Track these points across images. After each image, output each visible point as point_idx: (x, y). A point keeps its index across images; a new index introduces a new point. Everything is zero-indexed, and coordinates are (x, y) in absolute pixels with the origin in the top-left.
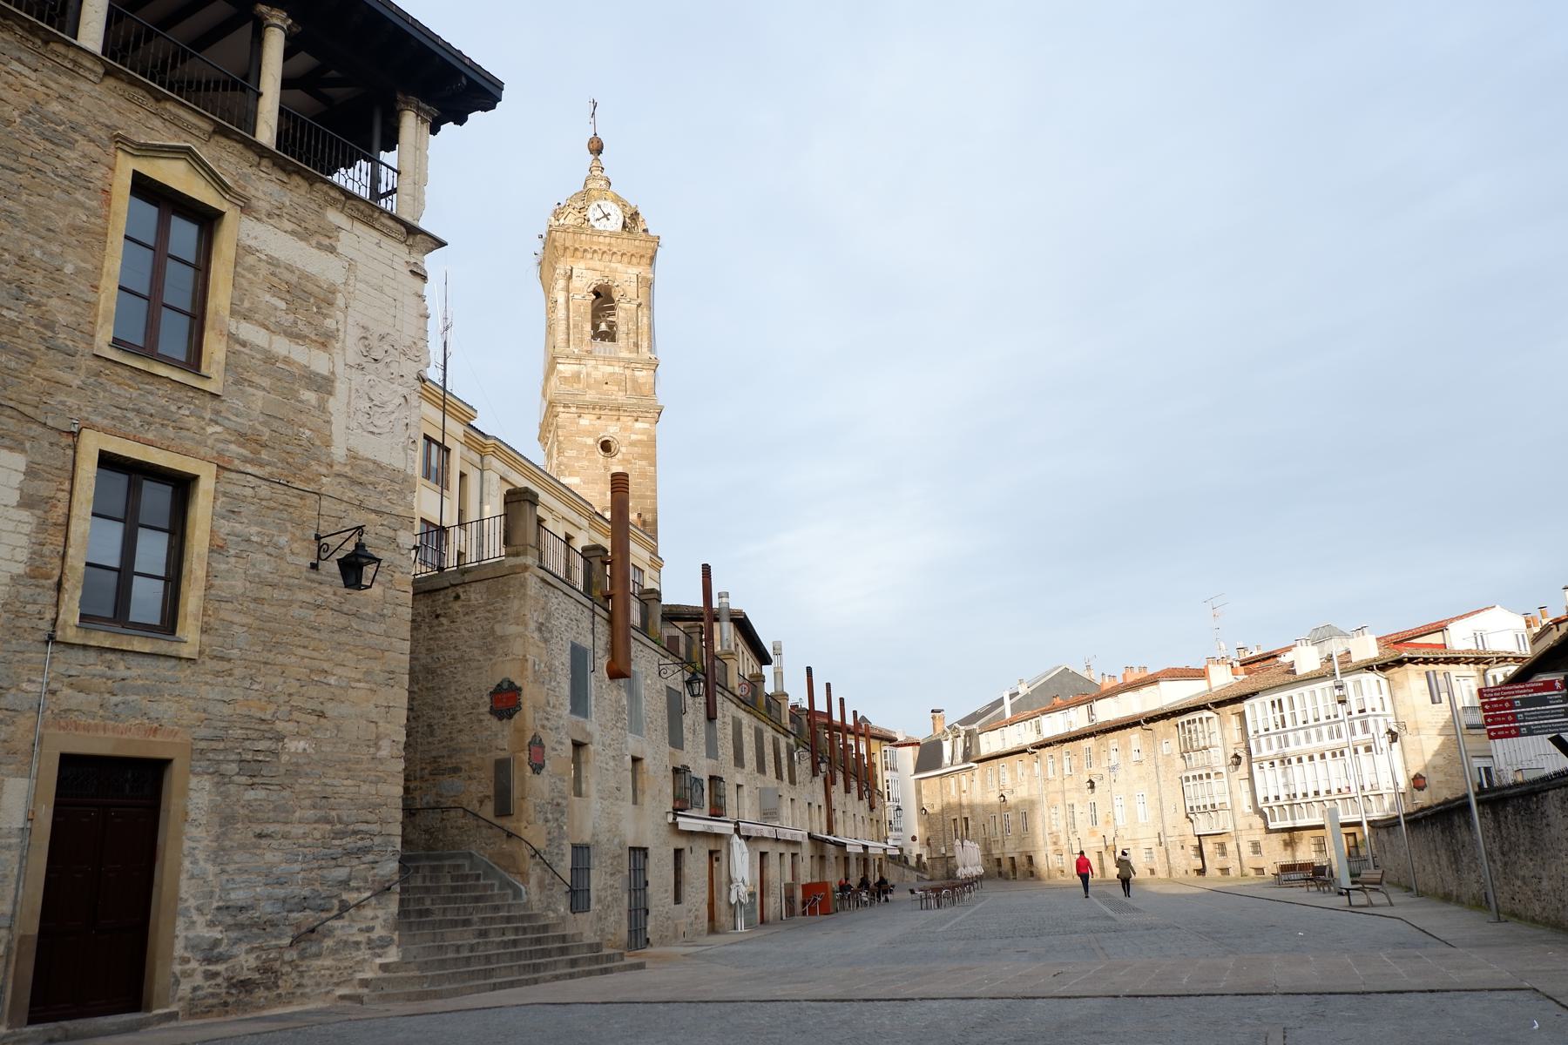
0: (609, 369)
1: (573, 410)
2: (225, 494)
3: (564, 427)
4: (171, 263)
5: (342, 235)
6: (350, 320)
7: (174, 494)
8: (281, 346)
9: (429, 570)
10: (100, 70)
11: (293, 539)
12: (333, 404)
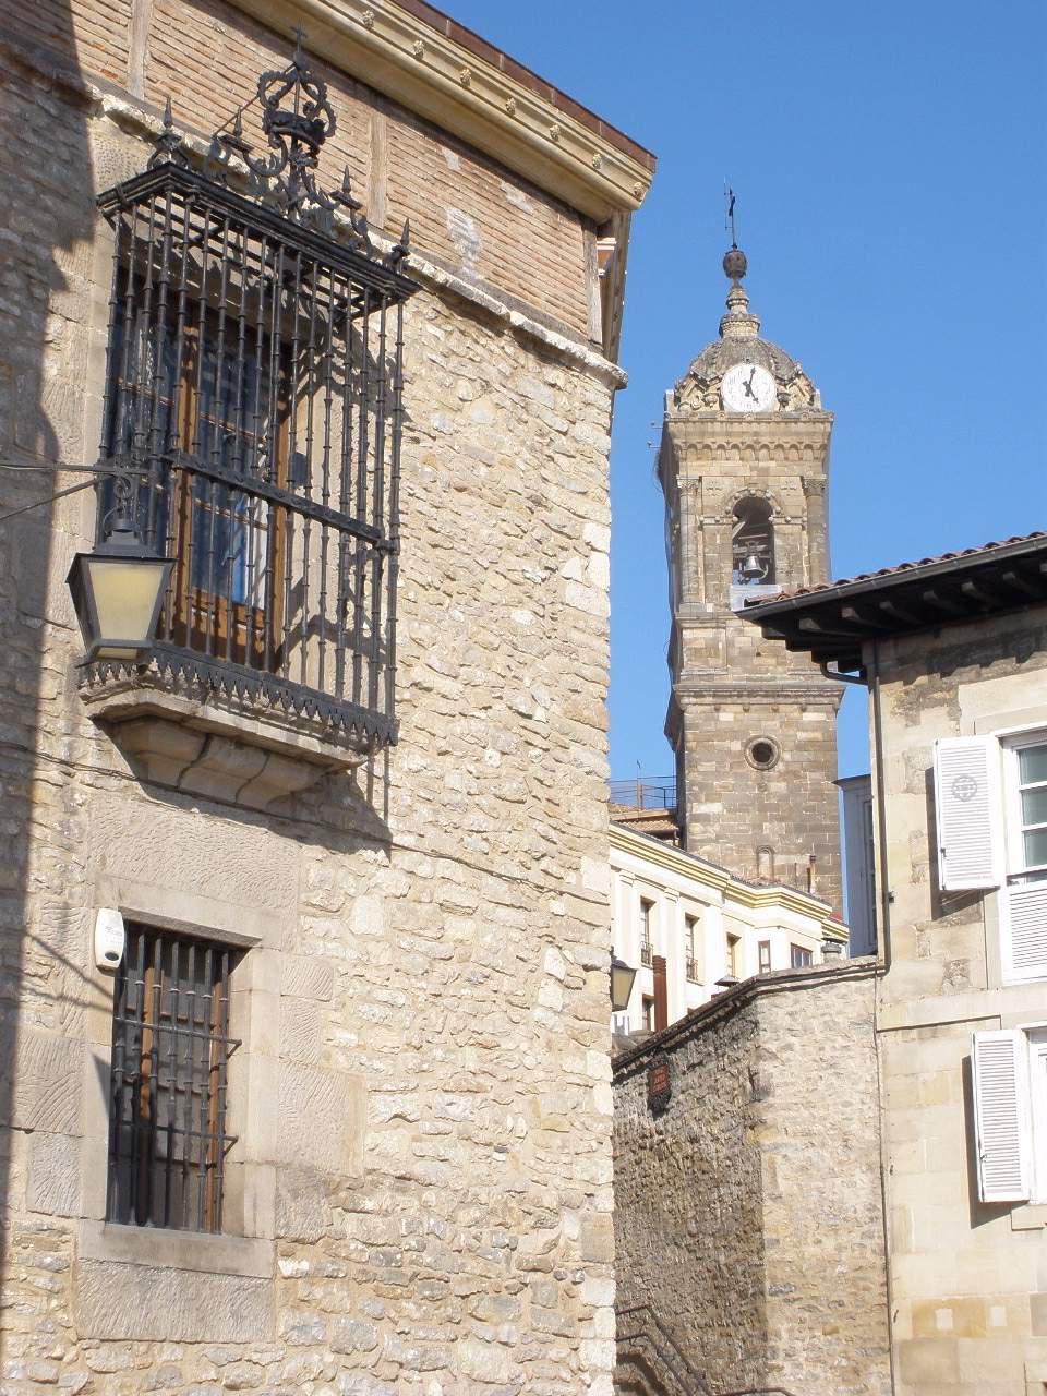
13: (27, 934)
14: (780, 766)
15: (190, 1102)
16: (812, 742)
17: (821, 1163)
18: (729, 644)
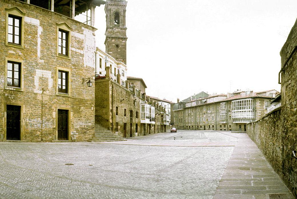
0: (118, 30)
1: (111, 39)
2: (72, 74)
3: (109, 42)
4: (63, 40)
5: (84, 31)
6: (86, 45)
7: (66, 74)
8: (77, 51)
9: (49, 42)
10: (54, 14)
11: (80, 79)
12: (84, 58)
13: (19, 27)
14: (120, 48)
15: (198, 115)
16: (123, 45)
17: (160, 168)
18: (114, 31)
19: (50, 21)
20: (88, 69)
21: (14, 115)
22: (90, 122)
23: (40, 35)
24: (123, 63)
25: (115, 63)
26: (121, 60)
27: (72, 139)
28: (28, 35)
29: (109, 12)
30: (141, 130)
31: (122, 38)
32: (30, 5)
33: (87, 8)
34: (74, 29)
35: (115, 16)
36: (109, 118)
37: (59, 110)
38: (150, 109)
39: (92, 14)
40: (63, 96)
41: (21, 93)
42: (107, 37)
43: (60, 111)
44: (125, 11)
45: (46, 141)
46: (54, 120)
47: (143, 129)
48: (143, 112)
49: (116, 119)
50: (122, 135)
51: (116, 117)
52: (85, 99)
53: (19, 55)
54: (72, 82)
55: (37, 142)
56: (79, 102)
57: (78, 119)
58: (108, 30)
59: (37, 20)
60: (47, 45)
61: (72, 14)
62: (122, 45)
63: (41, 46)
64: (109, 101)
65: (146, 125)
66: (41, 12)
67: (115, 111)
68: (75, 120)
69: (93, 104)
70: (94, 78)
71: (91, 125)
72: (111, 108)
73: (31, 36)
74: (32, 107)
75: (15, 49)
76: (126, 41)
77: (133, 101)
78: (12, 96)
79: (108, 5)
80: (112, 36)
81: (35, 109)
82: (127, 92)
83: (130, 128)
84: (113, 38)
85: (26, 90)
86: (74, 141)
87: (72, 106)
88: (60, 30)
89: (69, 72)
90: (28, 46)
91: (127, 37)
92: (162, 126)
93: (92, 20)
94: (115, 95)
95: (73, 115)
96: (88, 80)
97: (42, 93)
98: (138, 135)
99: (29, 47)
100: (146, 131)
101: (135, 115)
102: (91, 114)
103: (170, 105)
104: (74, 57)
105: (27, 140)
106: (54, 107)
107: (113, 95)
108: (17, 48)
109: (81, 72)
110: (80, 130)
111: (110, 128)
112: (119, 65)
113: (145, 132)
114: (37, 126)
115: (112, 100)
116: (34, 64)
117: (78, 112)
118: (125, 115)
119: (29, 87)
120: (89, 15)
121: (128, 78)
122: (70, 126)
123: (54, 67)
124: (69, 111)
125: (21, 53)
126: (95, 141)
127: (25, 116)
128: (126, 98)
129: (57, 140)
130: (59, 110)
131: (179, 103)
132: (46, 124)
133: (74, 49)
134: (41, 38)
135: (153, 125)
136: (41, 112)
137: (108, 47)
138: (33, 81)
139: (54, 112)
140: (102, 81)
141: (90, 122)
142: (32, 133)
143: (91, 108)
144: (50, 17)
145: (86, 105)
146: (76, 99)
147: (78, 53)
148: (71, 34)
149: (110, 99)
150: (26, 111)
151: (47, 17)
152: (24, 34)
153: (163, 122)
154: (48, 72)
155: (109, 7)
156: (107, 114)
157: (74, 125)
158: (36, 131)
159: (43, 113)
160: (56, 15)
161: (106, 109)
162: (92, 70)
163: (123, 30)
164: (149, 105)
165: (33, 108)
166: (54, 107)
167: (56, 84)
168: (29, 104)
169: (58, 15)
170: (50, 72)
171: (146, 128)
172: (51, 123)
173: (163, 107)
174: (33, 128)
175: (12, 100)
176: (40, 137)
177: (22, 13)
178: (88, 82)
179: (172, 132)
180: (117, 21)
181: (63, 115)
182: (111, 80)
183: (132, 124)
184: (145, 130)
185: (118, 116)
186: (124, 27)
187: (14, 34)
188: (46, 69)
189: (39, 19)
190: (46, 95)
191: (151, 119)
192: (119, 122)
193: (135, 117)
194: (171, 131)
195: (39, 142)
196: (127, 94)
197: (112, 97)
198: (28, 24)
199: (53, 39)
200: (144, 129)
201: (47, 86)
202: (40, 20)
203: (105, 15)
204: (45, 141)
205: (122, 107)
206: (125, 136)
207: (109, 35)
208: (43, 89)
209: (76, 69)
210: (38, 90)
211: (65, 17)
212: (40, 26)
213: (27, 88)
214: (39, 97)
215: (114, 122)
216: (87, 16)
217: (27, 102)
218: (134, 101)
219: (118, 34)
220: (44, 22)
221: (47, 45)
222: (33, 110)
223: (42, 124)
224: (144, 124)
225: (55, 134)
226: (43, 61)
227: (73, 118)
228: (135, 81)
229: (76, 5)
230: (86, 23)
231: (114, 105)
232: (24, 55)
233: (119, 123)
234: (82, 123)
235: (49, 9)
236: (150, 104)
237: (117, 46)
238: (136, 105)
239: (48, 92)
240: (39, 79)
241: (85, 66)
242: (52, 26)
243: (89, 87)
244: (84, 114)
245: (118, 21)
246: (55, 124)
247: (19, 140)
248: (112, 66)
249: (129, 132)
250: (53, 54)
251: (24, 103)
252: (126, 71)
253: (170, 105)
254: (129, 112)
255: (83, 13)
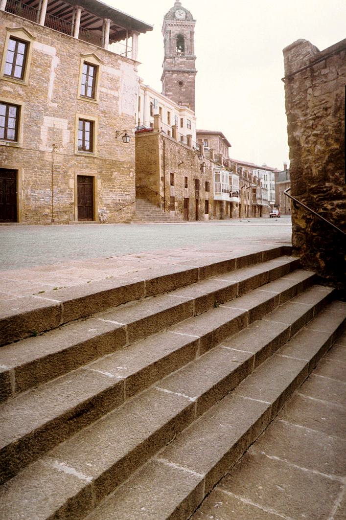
2: (100, 124)
8: (109, 92)
11: (112, 132)
12: (119, 103)
14: (184, 86)
18: (175, 62)
19: (72, 50)
20: (125, 118)
21: (7, 183)
22: (129, 195)
23: (55, 68)
24: (189, 109)
25: (176, 108)
26: (186, 104)
27: (100, 220)
28: (37, 67)
29: (168, 34)
30: (215, 211)
31: (188, 72)
32: (44, 28)
33: (127, 35)
34: (106, 62)
35: (177, 40)
36: (159, 189)
37: (78, 176)
38: (230, 179)
39: (134, 43)
40: (85, 157)
41: (19, 150)
42: (165, 71)
43: (81, 178)
44: (192, 33)
45: (59, 223)
46: (72, 191)
47: (218, 209)
48: (218, 183)
49: (171, 192)
50: (181, 216)
51: (171, 189)
52: (119, 161)
53: (19, 95)
54: (99, 135)
55: (46, 224)
56: (110, 165)
57: (110, 189)
58: (167, 60)
59: (52, 47)
60: (64, 82)
61: (104, 43)
62: (189, 82)
63: (55, 83)
64: (159, 165)
65: (225, 204)
66: (60, 37)
67: (168, 179)
68: (105, 192)
69: (132, 168)
70: (134, 130)
71: (130, 198)
72: (161, 175)
73: (41, 69)
74: (36, 173)
75: (14, 84)
76: (195, 76)
77: (199, 165)
78: (4, 154)
79: (166, 25)
80: (173, 69)
81: (41, 175)
82: (189, 151)
83: (195, 207)
84: (174, 72)
85: (27, 146)
86: (104, 222)
87: (99, 170)
88: (85, 63)
89: (94, 121)
90: (35, 82)
91: (196, 70)
92: (254, 207)
93: (134, 51)
94: (168, 155)
95: (102, 184)
96: (125, 133)
97: (53, 151)
98: (210, 219)
99: (36, 83)
100: (225, 213)
101: (205, 187)
102: (128, 183)
103: (274, 174)
104: (104, 101)
105: (28, 222)
106: (71, 172)
107: (166, 155)
108: (17, 84)
109: (113, 121)
110: (112, 206)
111: (161, 205)
112: (183, 113)
113: (221, 215)
114: (44, 201)
115: (164, 164)
116: (41, 108)
117: (108, 179)
118: (186, 187)
119: (30, 141)
120: (130, 44)
121: (198, 131)
122: (97, 199)
123: (72, 113)
124: (95, 178)
125: (23, 91)
126: (135, 222)
127: (25, 186)
128: (188, 160)
129: (77, 221)
130: (78, 176)
131: (287, 170)
132: (58, 196)
133: (103, 90)
134: (56, 73)
135: (237, 204)
136: (50, 180)
137: (166, 85)
138: (38, 133)
139: (70, 179)
140: (148, 135)
141: (129, 195)
142: (36, 212)
143: (130, 175)
144: (72, 45)
145: (122, 169)
146: (105, 160)
147: (110, 94)
148: (102, 69)
149: (161, 162)
150: (26, 177)
151: (67, 45)
152: (31, 65)
153: (256, 200)
154: (62, 120)
155: (169, 28)
156: (155, 183)
157: (104, 198)
158: (44, 207)
159: (54, 180)
160: (80, 44)
161: (154, 176)
162: (130, 119)
163: (191, 60)
164: (228, 173)
165: (38, 174)
166: (71, 172)
167: (74, 138)
168: (32, 167)
169: (84, 43)
170: (67, 121)
171: (224, 209)
172: (67, 196)
173: (255, 177)
174: (38, 203)
175: (3, 161)
176: (50, 216)
177: (30, 36)
178: (124, 136)
179: (271, 216)
180: (180, 47)
181: (86, 184)
182: (161, 134)
183: (199, 200)
184: (221, 210)
185: (173, 187)
186: (191, 56)
187: (14, 64)
188: (60, 116)
189: (55, 47)
190: (59, 154)
191: (230, 194)
192: (176, 196)
193: (205, 190)
194: (270, 215)
195: (49, 224)
196: (189, 155)
197: (163, 158)
198: (38, 52)
199: (74, 74)
200: (220, 209)
201: (61, 140)
202: (56, 48)
203: (163, 38)
204: (58, 222)
205: (181, 175)
206: (186, 218)
207: (168, 67)
208: (54, 145)
209: (105, 117)
210: (46, 146)
211: (93, 47)
212: (56, 56)
213: (29, 143)
214: (48, 158)
215: (168, 196)
216: (127, 46)
217: (28, 165)
218: (202, 166)
219: (182, 65)
220: (63, 52)
221: (64, 82)
222: (37, 176)
223: (52, 197)
224: (221, 202)
225: (73, 213)
226: (55, 105)
227: (101, 188)
228: (211, 136)
229: (112, 31)
230: (124, 55)
231: (166, 171)
232: (27, 95)
233: (176, 197)
234: (116, 195)
235: (72, 33)
236: (231, 171)
237: (181, 83)
238: (204, 171)
239: (61, 149)
240: (49, 130)
241: (120, 113)
242: (73, 58)
243: (126, 142)
244: (117, 182)
245: (183, 47)
246: (73, 197)
247: (16, 222)
248: (171, 113)
249: (194, 213)
250: (72, 96)
251: (24, 165)
252: (195, 120)
253: (273, 175)
254: (194, 182)
255: (122, 40)
